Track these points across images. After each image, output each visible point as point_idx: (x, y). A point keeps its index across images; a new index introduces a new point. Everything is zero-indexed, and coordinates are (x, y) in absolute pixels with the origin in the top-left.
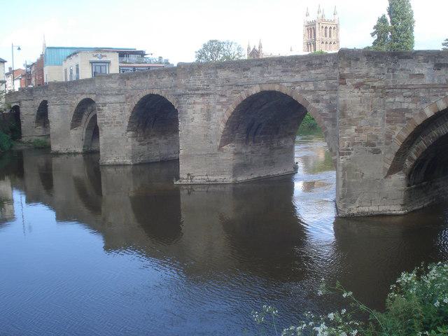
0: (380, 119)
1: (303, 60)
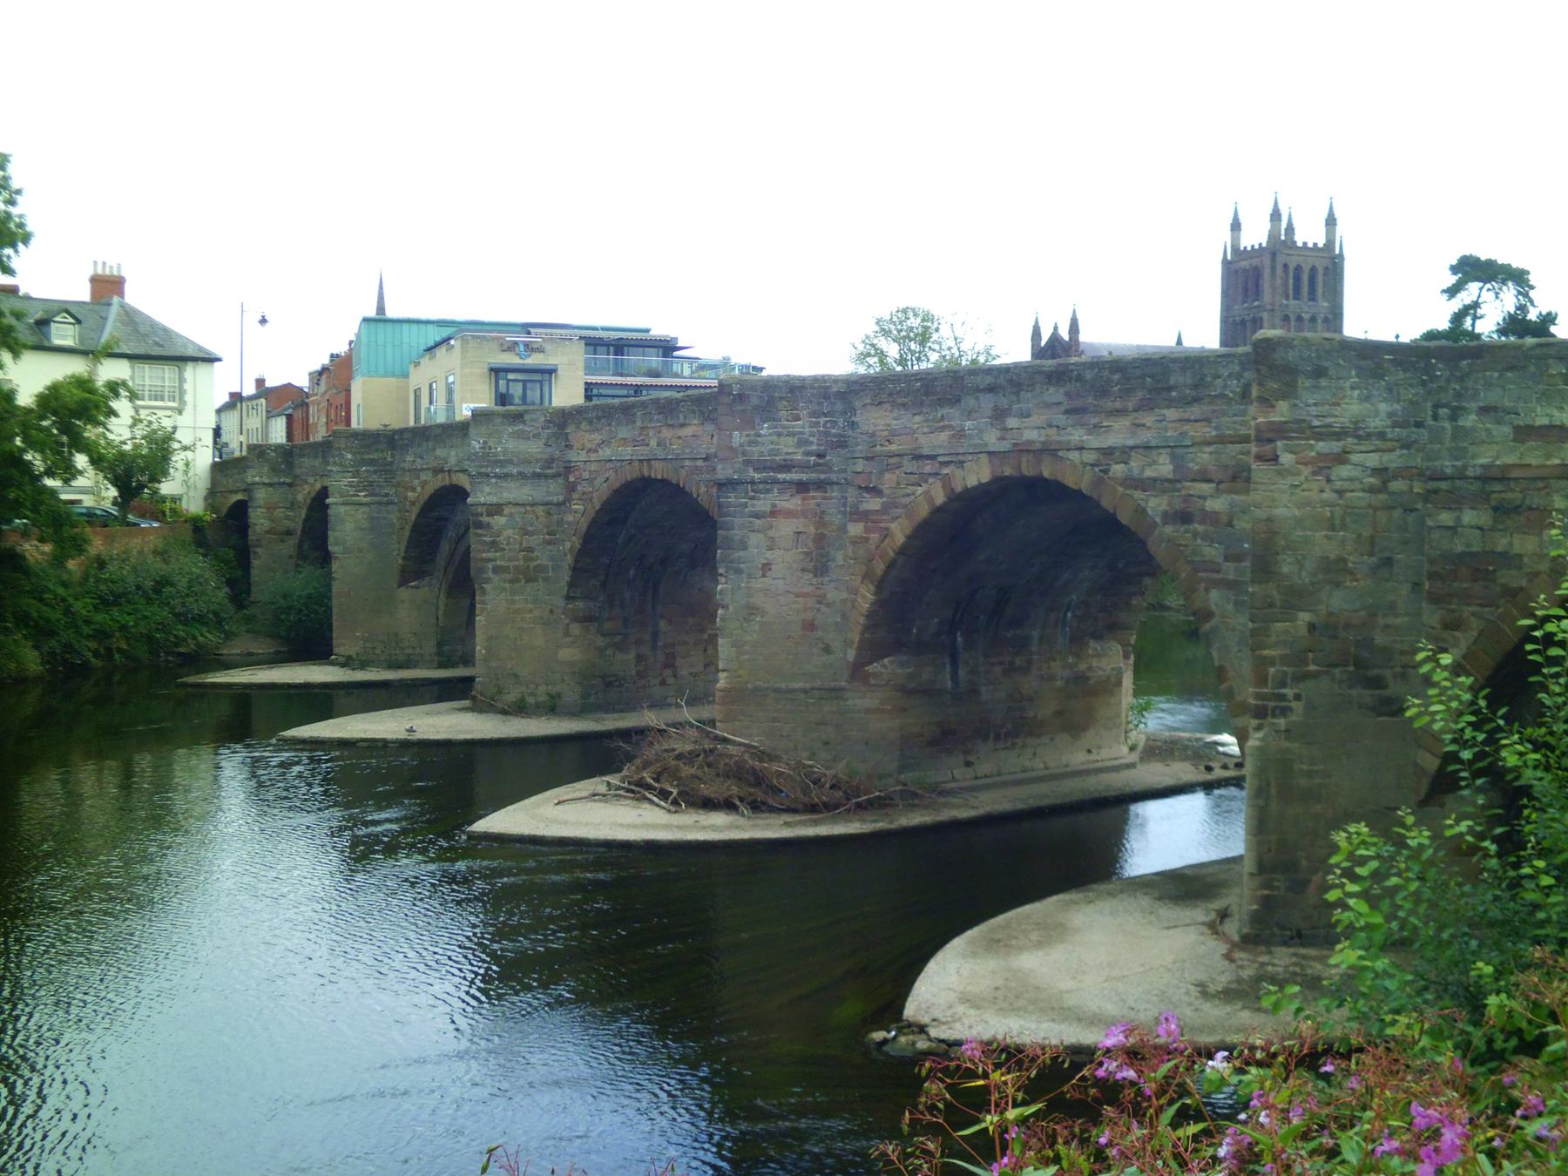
0: (1405, 590)
1: (1138, 372)
